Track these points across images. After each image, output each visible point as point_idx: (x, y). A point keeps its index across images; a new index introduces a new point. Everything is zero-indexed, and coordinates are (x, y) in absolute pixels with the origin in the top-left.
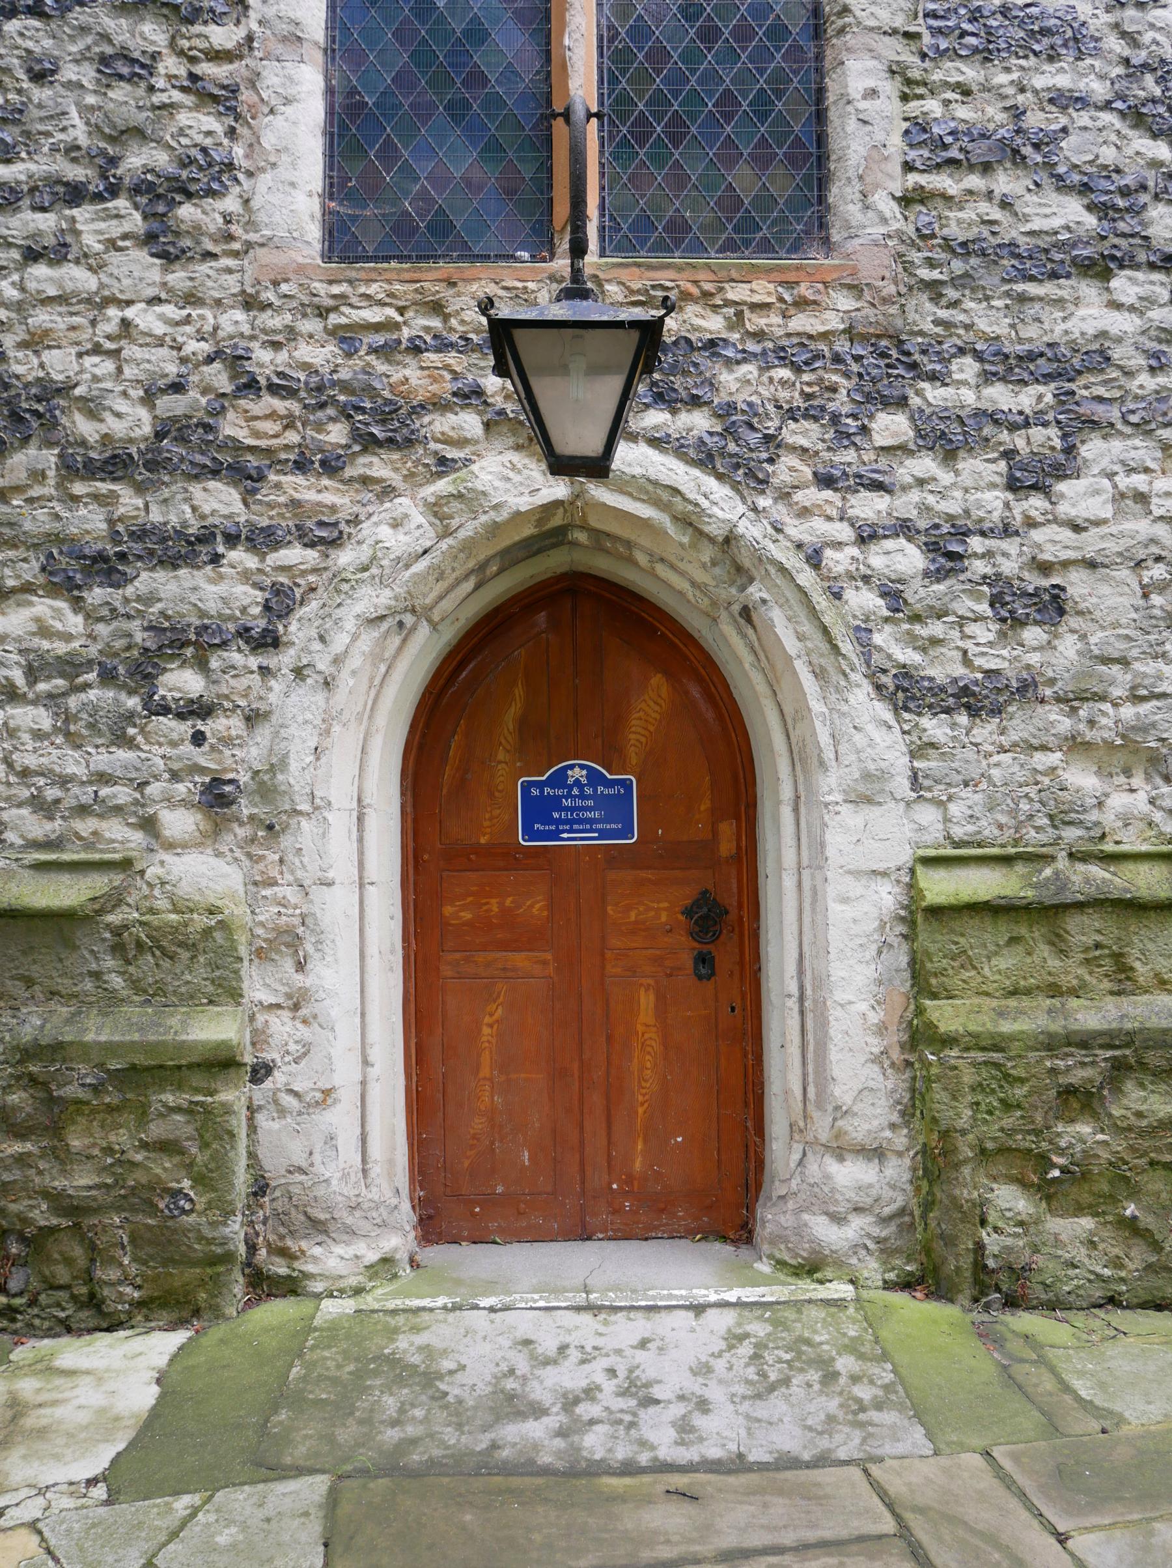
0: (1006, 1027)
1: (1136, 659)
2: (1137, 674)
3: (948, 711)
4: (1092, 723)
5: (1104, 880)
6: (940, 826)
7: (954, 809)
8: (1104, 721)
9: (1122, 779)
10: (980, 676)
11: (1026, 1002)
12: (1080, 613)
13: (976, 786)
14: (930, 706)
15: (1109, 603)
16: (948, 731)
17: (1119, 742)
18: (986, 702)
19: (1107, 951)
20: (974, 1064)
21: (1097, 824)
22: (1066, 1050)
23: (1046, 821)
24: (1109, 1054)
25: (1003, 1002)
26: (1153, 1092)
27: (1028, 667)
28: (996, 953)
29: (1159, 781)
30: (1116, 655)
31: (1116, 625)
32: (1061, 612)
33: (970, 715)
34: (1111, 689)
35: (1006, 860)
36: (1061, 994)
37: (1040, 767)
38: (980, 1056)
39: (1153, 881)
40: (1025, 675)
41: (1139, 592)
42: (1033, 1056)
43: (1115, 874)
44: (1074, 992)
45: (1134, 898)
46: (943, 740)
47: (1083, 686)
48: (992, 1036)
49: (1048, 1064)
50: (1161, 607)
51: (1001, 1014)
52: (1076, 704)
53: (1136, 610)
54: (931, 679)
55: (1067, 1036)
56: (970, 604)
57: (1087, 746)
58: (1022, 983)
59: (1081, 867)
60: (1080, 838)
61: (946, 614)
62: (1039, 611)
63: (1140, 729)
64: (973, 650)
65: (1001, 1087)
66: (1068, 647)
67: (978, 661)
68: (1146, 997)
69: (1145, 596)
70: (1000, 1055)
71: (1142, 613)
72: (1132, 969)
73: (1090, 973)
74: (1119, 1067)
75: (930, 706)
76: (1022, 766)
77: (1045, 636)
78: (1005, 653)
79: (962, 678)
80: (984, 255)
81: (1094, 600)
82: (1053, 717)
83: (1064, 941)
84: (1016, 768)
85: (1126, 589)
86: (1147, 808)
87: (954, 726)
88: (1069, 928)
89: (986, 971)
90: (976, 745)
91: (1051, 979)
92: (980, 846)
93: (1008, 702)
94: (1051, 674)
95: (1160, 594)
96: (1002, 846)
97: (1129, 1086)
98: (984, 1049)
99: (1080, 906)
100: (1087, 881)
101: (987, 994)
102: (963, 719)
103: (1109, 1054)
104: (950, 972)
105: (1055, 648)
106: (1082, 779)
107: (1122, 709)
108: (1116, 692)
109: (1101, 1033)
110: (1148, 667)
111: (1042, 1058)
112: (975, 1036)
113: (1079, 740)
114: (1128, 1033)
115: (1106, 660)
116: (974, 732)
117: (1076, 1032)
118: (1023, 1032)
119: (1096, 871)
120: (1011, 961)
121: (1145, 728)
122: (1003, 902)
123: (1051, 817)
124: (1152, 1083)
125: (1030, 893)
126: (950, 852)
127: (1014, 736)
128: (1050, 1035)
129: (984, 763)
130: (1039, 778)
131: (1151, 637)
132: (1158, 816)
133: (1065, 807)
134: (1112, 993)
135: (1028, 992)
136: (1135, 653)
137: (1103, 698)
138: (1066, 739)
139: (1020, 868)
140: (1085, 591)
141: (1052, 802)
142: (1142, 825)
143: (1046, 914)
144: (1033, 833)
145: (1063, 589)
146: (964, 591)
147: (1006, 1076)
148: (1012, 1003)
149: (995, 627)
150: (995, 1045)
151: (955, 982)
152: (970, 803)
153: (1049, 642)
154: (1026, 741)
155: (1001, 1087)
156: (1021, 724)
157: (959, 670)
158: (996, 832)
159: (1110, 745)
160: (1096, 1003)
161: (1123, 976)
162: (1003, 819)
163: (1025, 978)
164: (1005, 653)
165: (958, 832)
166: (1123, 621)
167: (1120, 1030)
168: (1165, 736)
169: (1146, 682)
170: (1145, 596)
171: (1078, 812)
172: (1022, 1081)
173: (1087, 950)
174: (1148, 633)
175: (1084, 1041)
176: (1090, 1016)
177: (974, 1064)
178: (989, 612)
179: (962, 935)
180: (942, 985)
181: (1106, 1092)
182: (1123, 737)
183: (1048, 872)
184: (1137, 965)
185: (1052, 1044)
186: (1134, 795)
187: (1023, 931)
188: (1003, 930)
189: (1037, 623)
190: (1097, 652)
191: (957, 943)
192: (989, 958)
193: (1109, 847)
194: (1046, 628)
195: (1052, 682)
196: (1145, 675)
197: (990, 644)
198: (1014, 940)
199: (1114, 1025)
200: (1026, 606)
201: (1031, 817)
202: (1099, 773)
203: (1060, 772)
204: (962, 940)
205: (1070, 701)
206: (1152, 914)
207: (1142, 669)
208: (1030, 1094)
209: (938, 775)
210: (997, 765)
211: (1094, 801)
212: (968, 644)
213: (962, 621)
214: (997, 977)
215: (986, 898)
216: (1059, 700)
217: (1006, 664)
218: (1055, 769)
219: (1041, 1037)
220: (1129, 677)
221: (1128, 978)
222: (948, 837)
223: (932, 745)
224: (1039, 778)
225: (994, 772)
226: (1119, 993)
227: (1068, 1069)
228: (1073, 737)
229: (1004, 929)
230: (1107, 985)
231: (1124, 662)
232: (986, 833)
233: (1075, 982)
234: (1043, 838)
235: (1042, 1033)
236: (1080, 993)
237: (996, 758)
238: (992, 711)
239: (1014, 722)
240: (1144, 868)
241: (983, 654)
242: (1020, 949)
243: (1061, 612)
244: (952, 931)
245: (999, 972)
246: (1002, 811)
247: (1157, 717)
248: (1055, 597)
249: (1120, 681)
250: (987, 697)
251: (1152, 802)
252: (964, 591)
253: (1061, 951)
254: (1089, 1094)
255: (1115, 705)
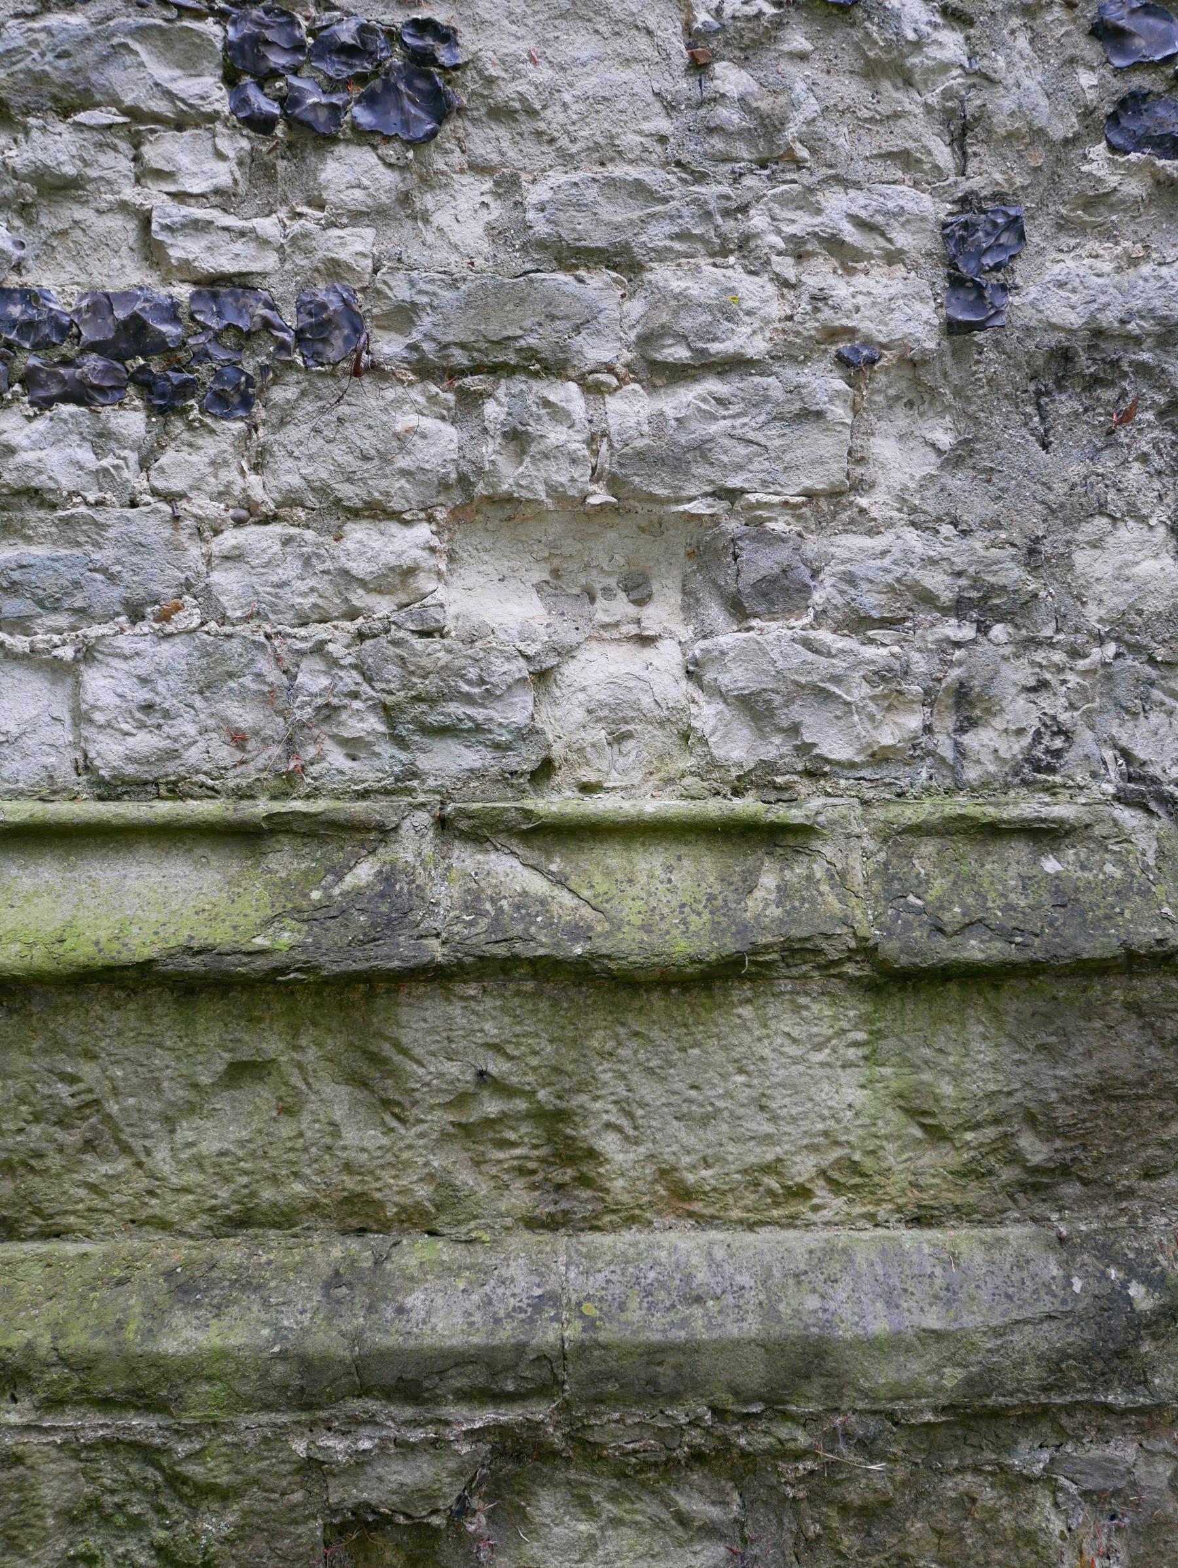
0: (186, 1336)
1: (661, 255)
2: (660, 298)
3: (81, 394)
4: (518, 439)
5: (523, 900)
6: (64, 735)
7: (101, 685)
8: (556, 435)
9: (620, 607)
10: (183, 292)
11: (274, 1250)
12: (501, 114)
13: (164, 617)
14: (29, 379)
15: (589, 84)
16: (86, 455)
17: (600, 496)
18: (203, 371)
19: (522, 1105)
20: (73, 1449)
21: (528, 734)
22: (355, 1406)
23: (374, 723)
24: (485, 1416)
25: (209, 1249)
26: (616, 1522)
27: (334, 269)
28: (191, 1109)
29: (715, 613)
30: (599, 239)
31: (607, 151)
32: (441, 108)
33: (153, 410)
34: (578, 341)
35: (244, 837)
36: (384, 1227)
37: (359, 568)
38: (93, 1425)
39: (666, 901)
40: (322, 292)
41: (680, 59)
42: (253, 1424)
43: (560, 881)
44: (420, 1220)
45: (595, 957)
46: (67, 481)
47: (495, 329)
48: (130, 1365)
49: (299, 1447)
50: (742, 100)
51: (185, 1288)
52: (472, 382)
53: (670, 108)
54: (30, 297)
55: (359, 1366)
56: (163, 73)
57: (508, 509)
58: (267, 1194)
59: (465, 858)
60: (475, 774)
61: (87, 102)
62: (370, 100)
63: (662, 461)
64: (166, 211)
65: (160, 1510)
66: (463, 217)
67: (182, 249)
68: (629, 1236)
69: (698, 67)
70: (151, 1422)
71: (687, 117)
72: (592, 1154)
73: (478, 1163)
74: (514, 1466)
75: (29, 379)
76: (307, 561)
77: (389, 178)
78: (267, 226)
79: (126, 296)
80: (1118, 893)
81: (544, 74)
82: (406, 420)
83: (392, 1073)
84: (291, 570)
85: (643, 43)
86: (677, 691)
87: (102, 439)
88: (406, 1038)
89: (161, 1159)
90: (170, 497)
91: (350, 1183)
92: (175, 792)
93: (276, 372)
94: (401, 291)
95: (743, 62)
96: (243, 794)
97: (546, 1505)
98: (106, 1403)
99: (437, 977)
100: (472, 902)
101: (163, 1225)
102: (131, 421)
103: (485, 1416)
104: (54, 1161)
105: (425, 217)
106: (495, 603)
107: (614, 404)
108: (597, 351)
109: (460, 1360)
110: (697, 281)
111: (281, 1432)
112: (83, 1365)
113: (480, 489)
114: (542, 1358)
115: (572, 256)
116: (167, 458)
117: (385, 1356)
118: (225, 1354)
119: (509, 872)
120: (238, 1132)
121: (676, 456)
122: (195, 964)
123: (388, 712)
124: (615, 1497)
125: (285, 938)
126: (91, 810)
127: (289, 475)
128: (307, 1365)
129: (195, 551)
130: (359, 598)
131: (709, 191)
132: (707, 715)
133: (430, 685)
134: (532, 1223)
135: (284, 1219)
136: (657, 235)
137: (553, 367)
138: (444, 486)
139: (284, 861)
140: (520, 48)
141: (393, 670)
142: (662, 739)
143: (340, 997)
144: (337, 758)
145: (447, 36)
146: (142, 33)
147: (176, 1481)
148: (232, 1252)
149: (235, 144)
150: (138, 1393)
151: (68, 1192)
152: (143, 667)
153: (405, 199)
154: (322, 490)
155: (160, 1510)
156: (308, 446)
157: (125, 274)
158: (225, 754)
159: (573, 506)
160: (480, 1256)
161: (570, 1173)
162: (245, 716)
163: (274, 1179)
164: (267, 226)
165: (110, 752)
166: (629, 140)
167: (520, 1349)
168: (735, 482)
169: (686, 323)
170: (698, 67)
171: (468, 699)
172: (225, 1495)
173: (462, 1100)
174: (701, 178)
175: (413, 1382)
176: (442, 1304)
177: (73, 1449)
178: (220, 99)
179: (90, 1055)
180: (26, 1198)
181: (476, 1525)
182: (614, 483)
183: (364, 873)
184: (609, 1144)
185: (312, 1388)
186: (648, 654)
187: (272, 1046)
188: (213, 1043)
189: (363, 136)
190: (542, 229)
191: (72, 1079)
192: (170, 1123)
193: (556, 802)
194: (390, 152)
195: (403, 316)
196: (684, 303)
197: (223, 197)
198: (242, 1072)
199: (506, 1334)
200: (333, 85)
201: (328, 712)
202: (553, 587)
203: (425, 583)
204: (88, 1071)
205: (460, 373)
206: (657, 1000)
207: (677, 285)
208: (242, 1533)
209: (48, 583)
210: (235, 557)
211: (520, 668)
212: (154, 197)
213: (138, 124)
214: (192, 1177)
215: (146, 953)
216: (424, 370)
217: (269, 261)
218: (410, 572)
219: (279, 1370)
220: (636, 307)
221: (584, 1181)
222: (85, 767)
223: (35, 496)
224: (359, 598)
225: (225, 580)
226: (552, 1224)
227: (361, 1461)
228: (464, 481)
229: (211, 1039)
230: (519, 1198)
231: (623, 262)
232: (193, 755)
233: (423, 1192)
234: (366, 772)
235: (282, 1356)
236: (439, 1224)
237: (230, 538)
238: (221, 399)
239: (293, 433)
240: (650, 863)
241: (198, 227)
242: (263, 1096)
243: (441, 108)
244: (57, 1044)
245: (198, 1162)
246: (243, 695)
247: (714, 428)
248: (421, 60)
249: (608, 317)
250: (203, 356)
251: (693, 673)
252: (142, 33)
253: (386, 1103)
254: (422, 1532)
255: (593, 390)
